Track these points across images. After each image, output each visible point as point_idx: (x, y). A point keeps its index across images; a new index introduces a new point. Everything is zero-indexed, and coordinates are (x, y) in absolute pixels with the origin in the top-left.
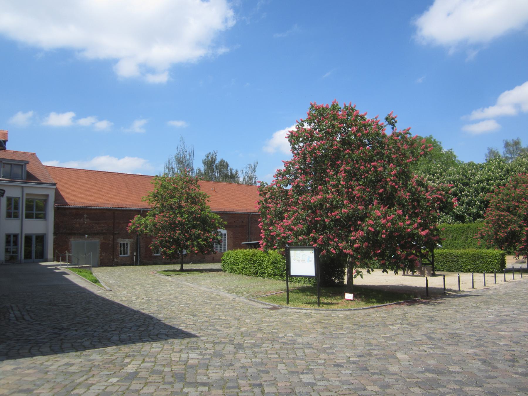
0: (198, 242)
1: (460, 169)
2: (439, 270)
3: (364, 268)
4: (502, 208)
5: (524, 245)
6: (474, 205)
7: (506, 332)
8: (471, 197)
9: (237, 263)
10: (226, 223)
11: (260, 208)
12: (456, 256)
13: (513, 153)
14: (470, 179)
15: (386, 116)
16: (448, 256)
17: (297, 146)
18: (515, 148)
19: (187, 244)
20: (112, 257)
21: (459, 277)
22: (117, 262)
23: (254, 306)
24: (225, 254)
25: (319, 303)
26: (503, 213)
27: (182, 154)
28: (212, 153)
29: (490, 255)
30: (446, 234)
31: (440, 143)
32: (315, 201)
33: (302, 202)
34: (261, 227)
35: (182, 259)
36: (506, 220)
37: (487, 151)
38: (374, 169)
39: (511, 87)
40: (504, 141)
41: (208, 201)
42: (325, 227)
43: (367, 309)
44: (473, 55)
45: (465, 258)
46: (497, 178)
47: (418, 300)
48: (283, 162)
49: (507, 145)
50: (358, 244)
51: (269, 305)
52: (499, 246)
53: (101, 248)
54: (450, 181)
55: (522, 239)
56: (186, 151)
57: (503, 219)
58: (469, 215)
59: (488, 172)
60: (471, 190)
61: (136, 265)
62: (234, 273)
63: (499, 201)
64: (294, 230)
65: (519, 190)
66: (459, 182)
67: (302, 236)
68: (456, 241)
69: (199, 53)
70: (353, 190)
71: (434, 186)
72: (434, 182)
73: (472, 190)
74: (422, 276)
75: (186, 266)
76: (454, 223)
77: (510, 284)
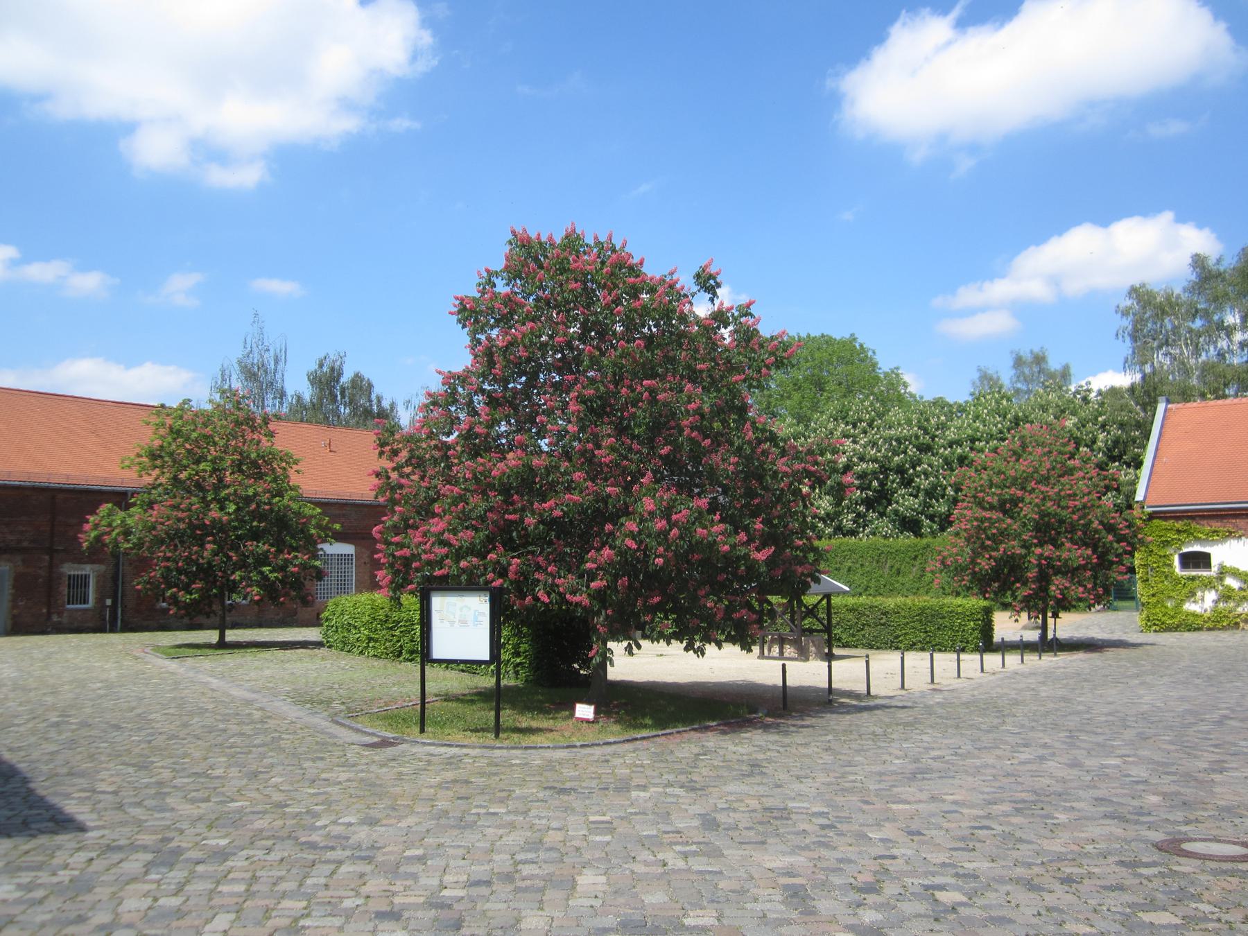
0: (262, 573)
1: (913, 413)
2: (846, 646)
3: (619, 641)
4: (988, 503)
5: (1033, 589)
6: (943, 497)
7: (909, 803)
8: (937, 477)
9: (355, 627)
10: (337, 526)
11: (380, 488)
12: (885, 613)
13: (1032, 380)
14: (933, 438)
15: (696, 269)
16: (868, 613)
17: (483, 337)
18: (1036, 369)
19: (232, 578)
20: (44, 611)
21: (902, 659)
22: (60, 623)
23: (336, 737)
24: (330, 603)
25: (497, 730)
26: (988, 514)
27: (256, 355)
28: (332, 357)
29: (960, 610)
30: (878, 562)
31: (874, 353)
32: (504, 473)
33: (475, 475)
34: (377, 536)
35: (223, 618)
36: (994, 531)
37: (976, 376)
38: (650, 395)
39: (1040, 238)
40: (1012, 352)
41: (298, 472)
42: (526, 540)
43: (615, 743)
44: (965, 164)
45: (905, 617)
46: (992, 436)
47: (755, 718)
48: (440, 373)
49: (1019, 362)
50: (601, 580)
51: (373, 734)
52: (980, 589)
53: (14, 587)
54: (891, 439)
55: (1029, 574)
56: (268, 350)
57: (990, 527)
58: (931, 518)
59: (975, 422)
60: (937, 461)
61: (113, 630)
62: (349, 651)
63: (982, 486)
64: (454, 546)
65: (1025, 463)
66: (910, 443)
67: (469, 559)
68: (900, 579)
69: (349, 124)
70: (599, 447)
71: (854, 450)
72: (855, 442)
73: (938, 461)
74: (801, 660)
75: (232, 635)
76: (898, 537)
77: (992, 678)
